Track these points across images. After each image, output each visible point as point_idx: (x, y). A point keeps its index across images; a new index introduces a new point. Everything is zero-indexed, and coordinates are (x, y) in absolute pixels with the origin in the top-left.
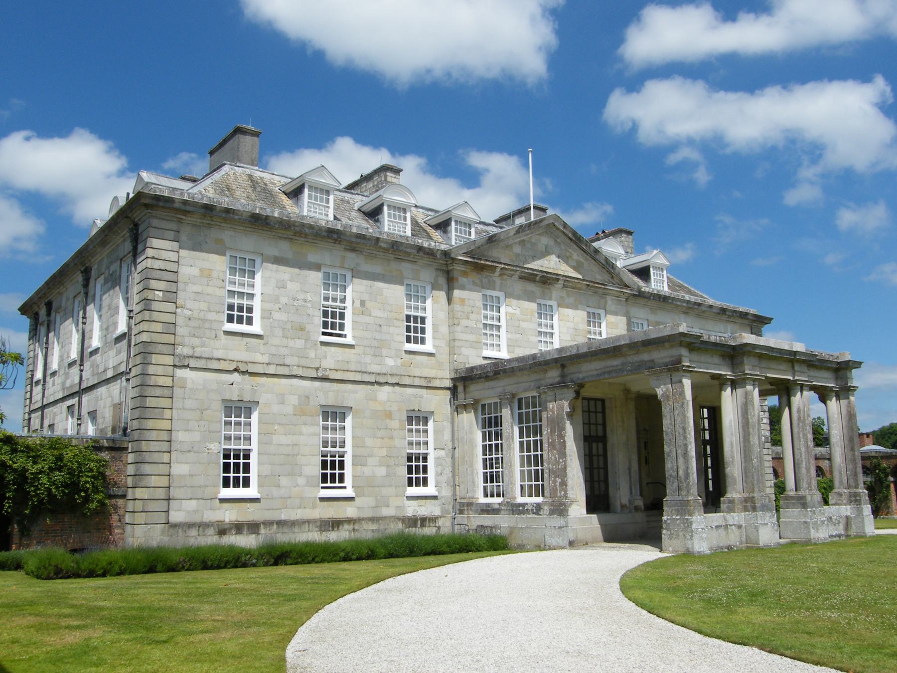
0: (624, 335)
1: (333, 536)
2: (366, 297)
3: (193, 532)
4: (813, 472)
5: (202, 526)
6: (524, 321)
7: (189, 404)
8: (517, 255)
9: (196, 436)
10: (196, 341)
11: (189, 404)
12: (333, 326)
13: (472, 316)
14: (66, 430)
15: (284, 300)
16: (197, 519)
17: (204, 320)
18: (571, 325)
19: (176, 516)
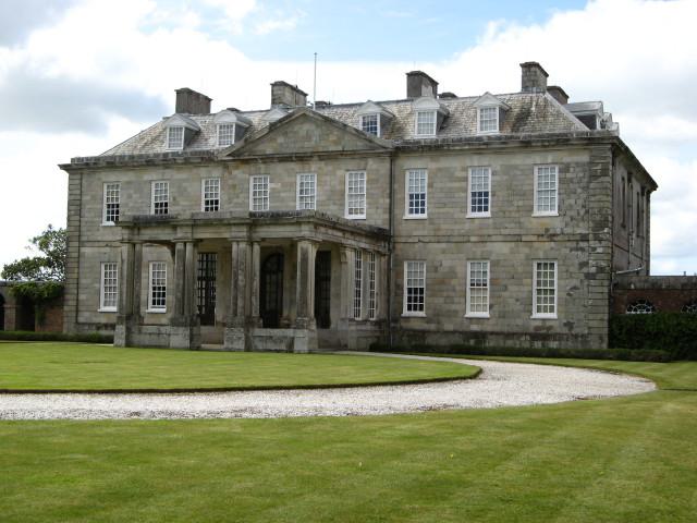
0: (645, 258)
1: (510, 343)
2: (176, 195)
3: (86, 327)
4: (354, 283)
5: (90, 324)
6: (285, 191)
7: (86, 265)
8: (281, 144)
9: (89, 281)
10: (89, 233)
11: (86, 265)
12: (545, 283)
13: (241, 195)
14: (602, 320)
15: (131, 205)
16: (89, 321)
17: (92, 222)
18: (327, 188)
19: (81, 320)
